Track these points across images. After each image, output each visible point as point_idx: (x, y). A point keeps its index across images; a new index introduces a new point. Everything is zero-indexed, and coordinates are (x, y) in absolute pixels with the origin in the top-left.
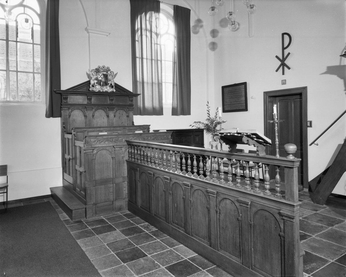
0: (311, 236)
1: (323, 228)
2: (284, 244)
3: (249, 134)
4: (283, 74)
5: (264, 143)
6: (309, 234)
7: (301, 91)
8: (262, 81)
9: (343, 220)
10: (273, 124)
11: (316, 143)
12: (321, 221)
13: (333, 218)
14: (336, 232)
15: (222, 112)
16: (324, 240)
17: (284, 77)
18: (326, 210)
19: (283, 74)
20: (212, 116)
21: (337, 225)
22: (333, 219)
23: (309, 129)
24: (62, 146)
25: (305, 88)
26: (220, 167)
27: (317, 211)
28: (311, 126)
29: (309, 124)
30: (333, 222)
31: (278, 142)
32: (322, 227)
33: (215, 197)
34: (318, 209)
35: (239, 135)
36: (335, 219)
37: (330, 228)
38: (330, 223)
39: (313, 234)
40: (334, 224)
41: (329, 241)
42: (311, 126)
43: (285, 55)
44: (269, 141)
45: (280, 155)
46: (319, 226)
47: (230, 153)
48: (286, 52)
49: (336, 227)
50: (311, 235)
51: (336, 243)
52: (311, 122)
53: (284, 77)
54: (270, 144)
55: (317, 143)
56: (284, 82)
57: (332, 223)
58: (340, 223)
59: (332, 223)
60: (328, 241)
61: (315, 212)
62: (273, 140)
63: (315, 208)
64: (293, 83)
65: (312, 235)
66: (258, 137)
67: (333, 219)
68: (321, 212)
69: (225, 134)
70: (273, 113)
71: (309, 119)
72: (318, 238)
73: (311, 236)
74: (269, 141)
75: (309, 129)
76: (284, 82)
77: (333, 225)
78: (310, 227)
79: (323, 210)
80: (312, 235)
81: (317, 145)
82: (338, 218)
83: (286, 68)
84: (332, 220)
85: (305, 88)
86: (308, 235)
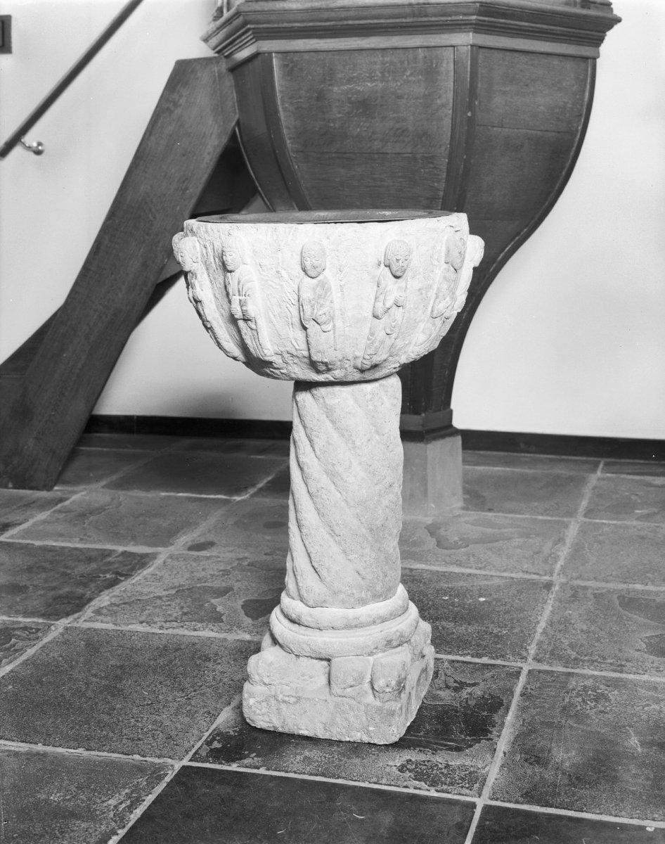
2: (307, 550)
9: (147, 555)
11: (31, 139)
13: (88, 557)
18: (60, 511)
21: (104, 599)
22: (90, 560)
26: (363, 619)
33: (551, 575)
34: (11, 518)
36: (105, 554)
37: (64, 622)
40: (88, 594)
49: (98, 612)
51: (78, 742)
55: (40, 144)
57: (80, 590)
58: (127, 576)
59: (80, 590)
67: (90, 560)
68: (27, 533)
77: (77, 604)
79: (42, 516)
81: (38, 153)
82: (121, 549)
84: (82, 569)
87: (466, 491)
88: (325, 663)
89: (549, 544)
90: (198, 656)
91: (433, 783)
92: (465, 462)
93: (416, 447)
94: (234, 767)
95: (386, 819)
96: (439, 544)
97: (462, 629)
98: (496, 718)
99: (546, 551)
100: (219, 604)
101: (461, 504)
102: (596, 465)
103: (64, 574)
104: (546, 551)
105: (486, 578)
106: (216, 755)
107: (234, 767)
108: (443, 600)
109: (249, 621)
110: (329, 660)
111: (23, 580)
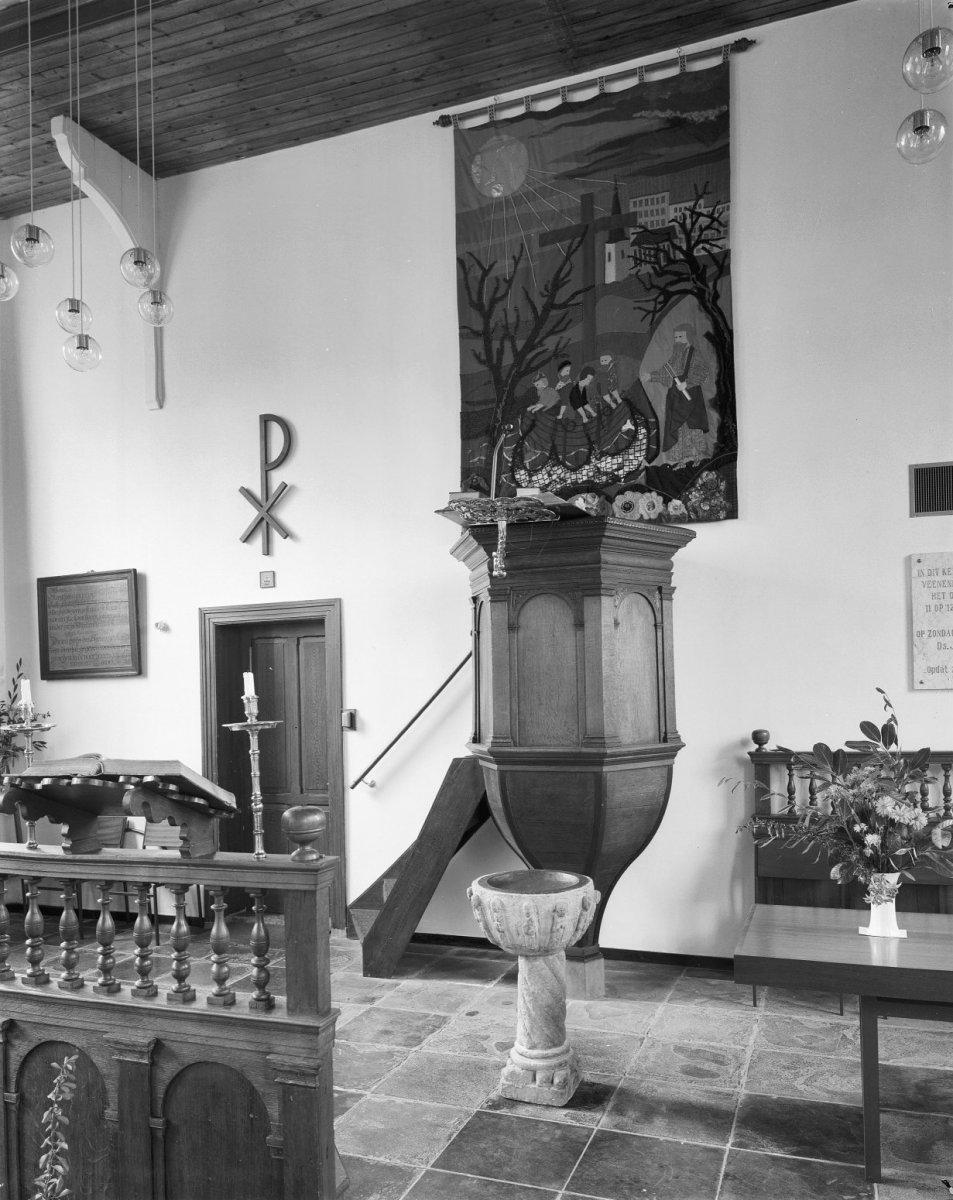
0: (361, 1096)
1: (392, 1055)
3: (149, 779)
4: (267, 551)
5: (211, 807)
6: (353, 1091)
7: (321, 614)
8: (194, 576)
10: (242, 738)
11: (368, 779)
12: (387, 1032)
14: (431, 1060)
15: (735, 521)
16: (399, 1101)
17: (267, 564)
19: (267, 551)
20: (608, 526)
22: (419, 1019)
23: (350, 735)
24: (143, 659)
25: (335, 604)
27: (373, 1000)
28: (353, 726)
29: (346, 722)
30: (419, 1029)
31: (262, 801)
32: (390, 1054)
34: (375, 995)
35: (110, 783)
38: (412, 1033)
39: (365, 1088)
41: (412, 1101)
42: (353, 726)
43: (275, 486)
44: (228, 798)
45: (268, 849)
46: (380, 1055)
47: (70, 856)
48: (277, 478)
50: (359, 1092)
52: (352, 717)
53: (267, 564)
54: (229, 810)
56: (269, 580)
60: (408, 1101)
61: (368, 1006)
62: (242, 791)
63: (365, 991)
64: (294, 579)
65: (363, 1092)
66: (187, 788)
69: (46, 781)
70: (243, 694)
71: (350, 704)
72: (382, 1098)
73: (361, 1096)
74: (228, 798)
75: (350, 737)
76: (269, 580)
78: (356, 1064)
80: (363, 1092)
83: (276, 536)
85: (335, 604)
86: (352, 1095)
87: (607, 986)
88: (55, 667)
89: (647, 1016)
90: (481, 1068)
91: (578, 1121)
92: (606, 967)
93: (579, 966)
94: (498, 1112)
95: (558, 1132)
96: (590, 1016)
97: (596, 1060)
98: (606, 1098)
99: (644, 1021)
100: (485, 1044)
101: (604, 993)
102: (682, 971)
103: (409, 1026)
104: (644, 1021)
105: (611, 1034)
106: (490, 1107)
107: (498, 1112)
108: (888, 862)
109: (498, 1052)
110: (266, 422)
111: (390, 1028)
